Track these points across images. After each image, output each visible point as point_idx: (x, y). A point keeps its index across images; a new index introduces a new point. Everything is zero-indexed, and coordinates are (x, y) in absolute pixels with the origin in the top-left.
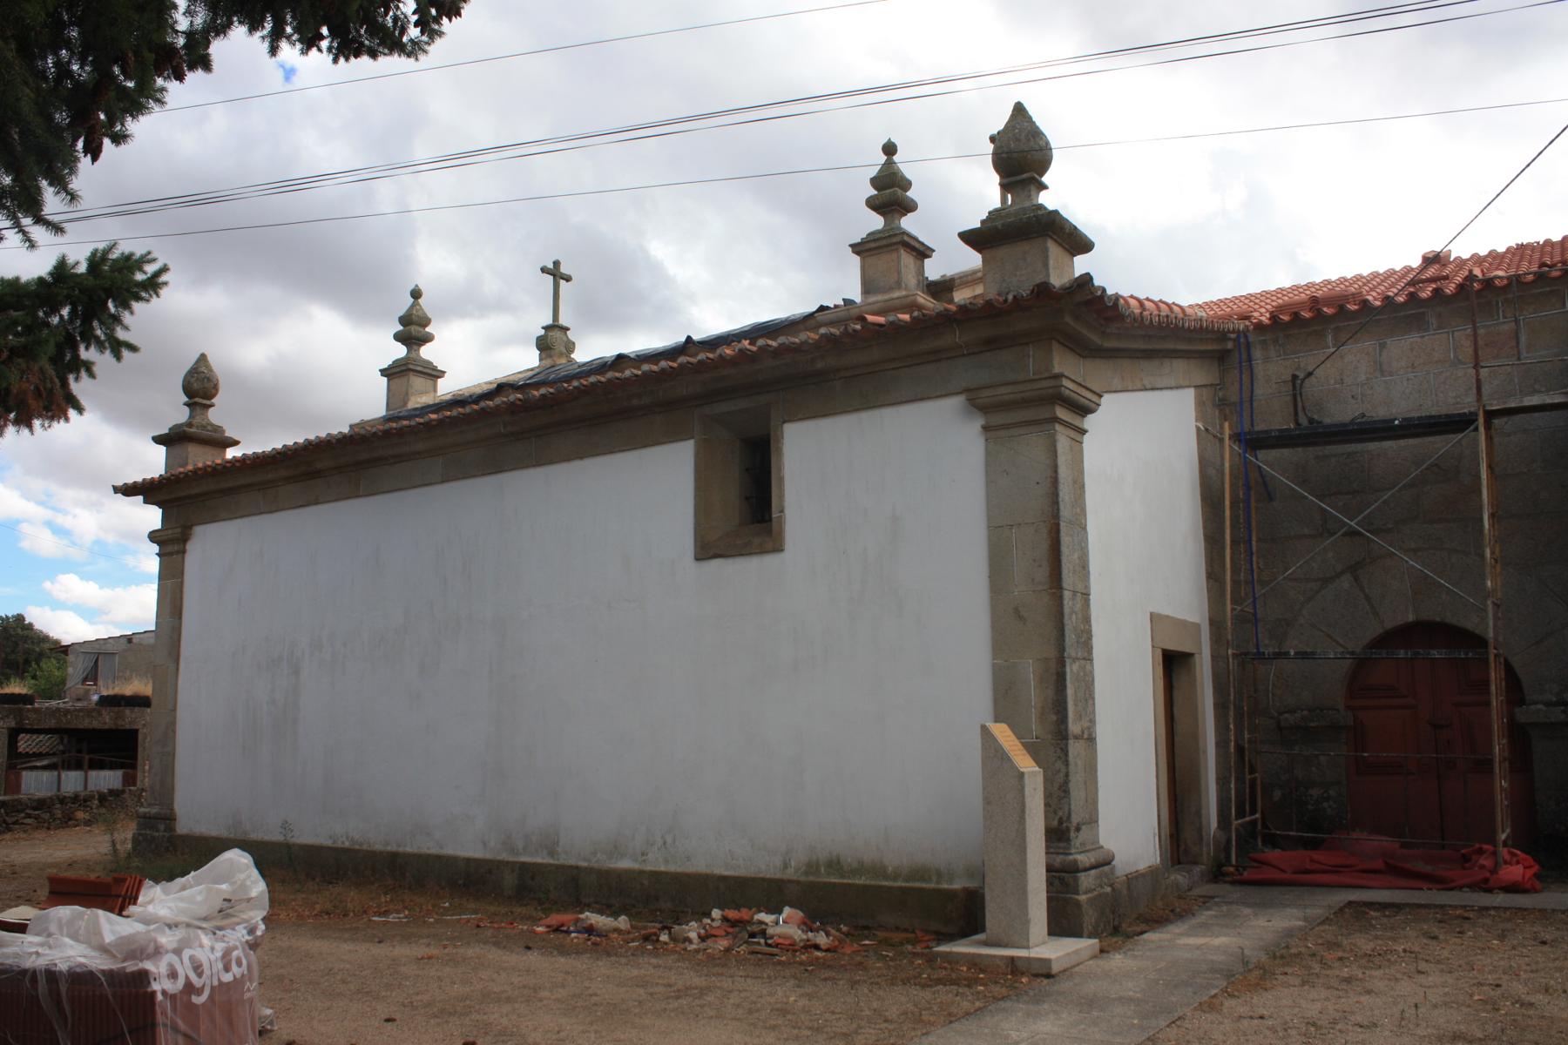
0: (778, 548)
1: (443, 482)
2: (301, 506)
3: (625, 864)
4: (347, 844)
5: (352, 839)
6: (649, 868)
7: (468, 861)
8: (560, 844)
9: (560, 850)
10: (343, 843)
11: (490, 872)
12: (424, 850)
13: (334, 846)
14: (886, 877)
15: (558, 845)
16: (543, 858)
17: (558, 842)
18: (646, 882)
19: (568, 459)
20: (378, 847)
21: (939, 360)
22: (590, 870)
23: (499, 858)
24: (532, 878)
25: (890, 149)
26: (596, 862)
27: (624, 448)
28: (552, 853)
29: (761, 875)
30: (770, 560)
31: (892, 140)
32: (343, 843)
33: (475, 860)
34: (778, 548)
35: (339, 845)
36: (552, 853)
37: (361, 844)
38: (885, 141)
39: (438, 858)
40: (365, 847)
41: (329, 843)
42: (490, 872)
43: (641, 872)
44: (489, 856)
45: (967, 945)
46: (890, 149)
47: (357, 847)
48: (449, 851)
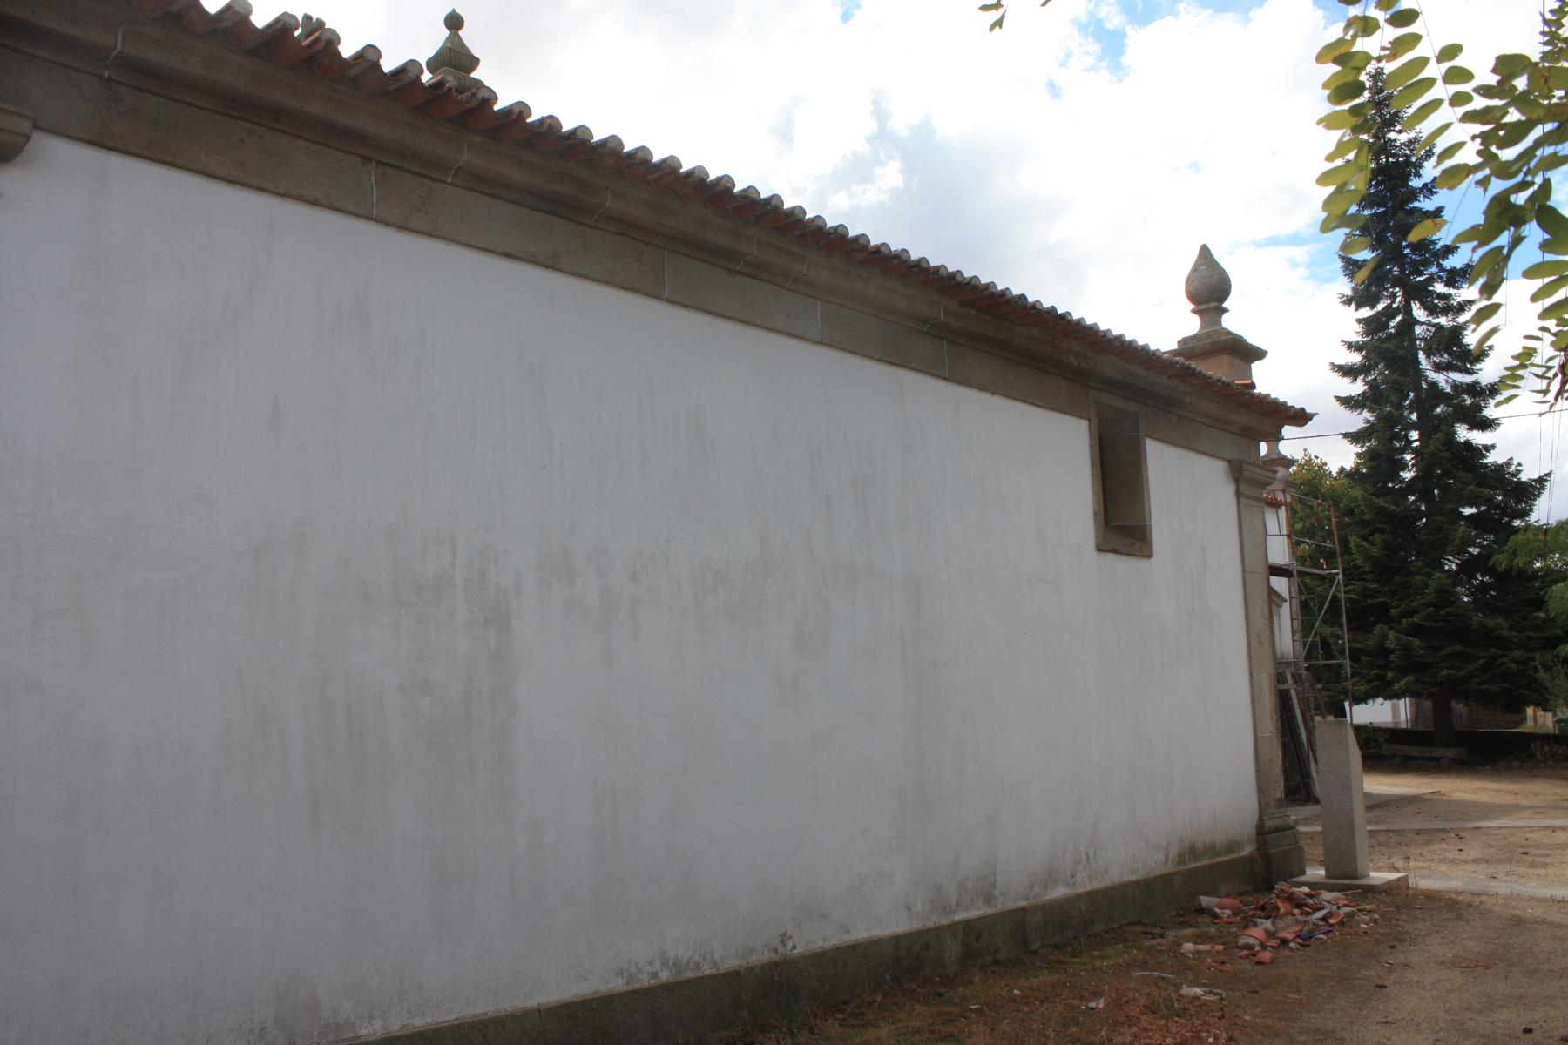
0: (1150, 556)
1: (821, 343)
2: (507, 255)
3: (1059, 892)
4: (665, 976)
5: (677, 964)
6: (1080, 890)
7: (897, 939)
8: (997, 886)
9: (997, 892)
10: (655, 975)
11: (928, 946)
12: (819, 944)
13: (630, 988)
14: (1218, 854)
15: (995, 888)
16: (979, 909)
17: (995, 881)
18: (1083, 907)
19: (981, 387)
20: (733, 963)
21: (1223, 430)
22: (1036, 908)
23: (930, 924)
24: (977, 939)
25: (454, 22)
26: (1034, 897)
27: (1035, 402)
28: (989, 900)
29: (1153, 874)
30: (1143, 562)
31: (457, 11)
32: (655, 975)
33: (906, 936)
34: (1150, 556)
35: (645, 980)
36: (989, 900)
37: (698, 966)
38: (449, 11)
39: (853, 948)
40: (707, 970)
41: (618, 985)
42: (928, 946)
43: (1079, 896)
44: (916, 925)
45: (1379, 878)
46: (454, 22)
47: (689, 975)
48: (860, 934)
